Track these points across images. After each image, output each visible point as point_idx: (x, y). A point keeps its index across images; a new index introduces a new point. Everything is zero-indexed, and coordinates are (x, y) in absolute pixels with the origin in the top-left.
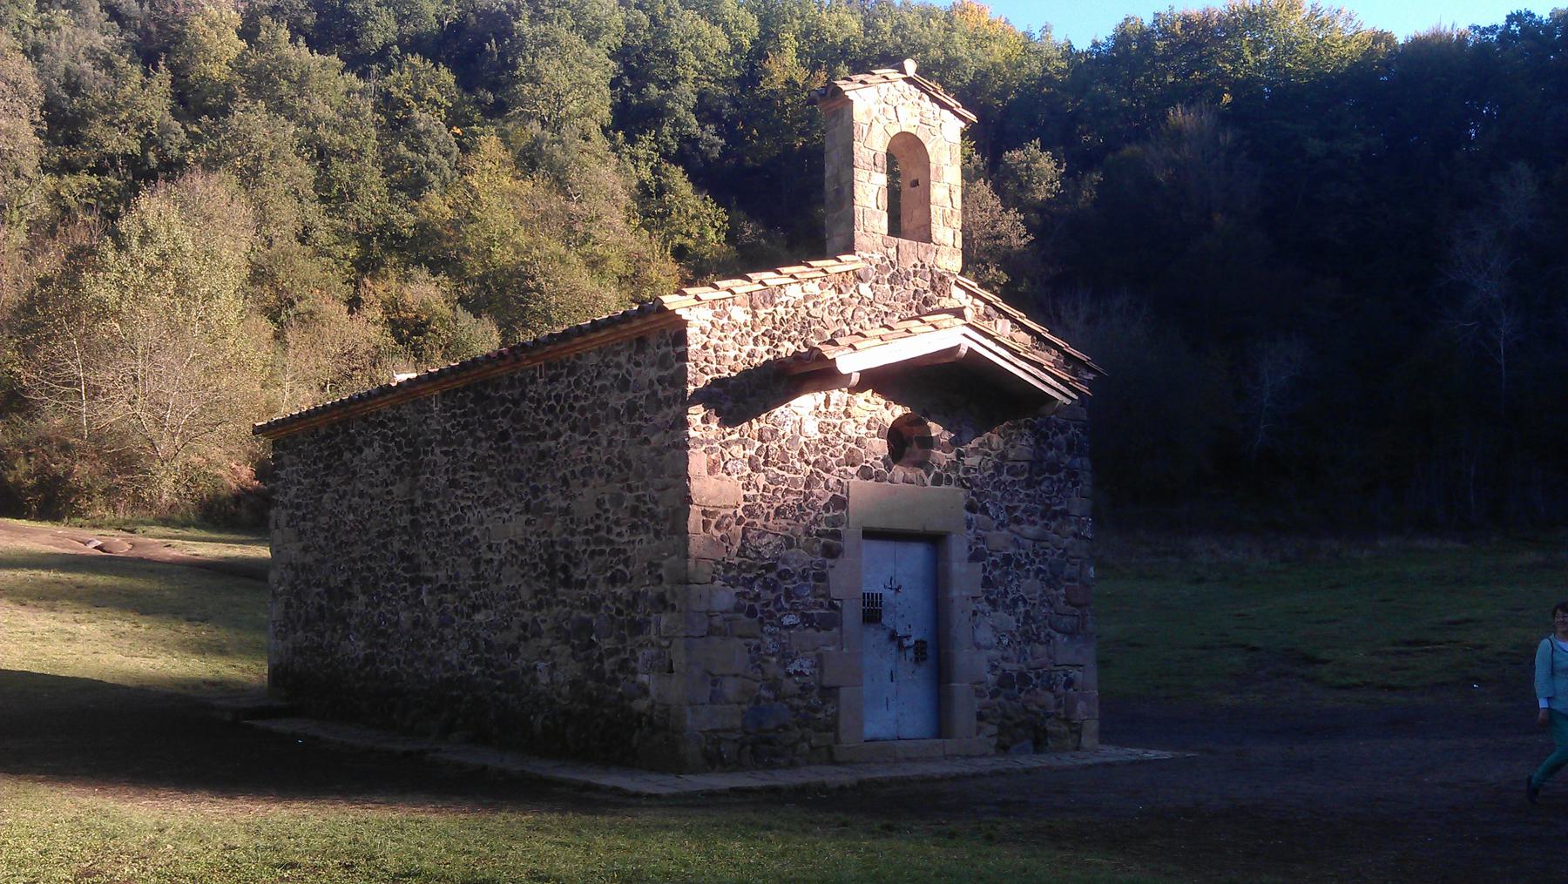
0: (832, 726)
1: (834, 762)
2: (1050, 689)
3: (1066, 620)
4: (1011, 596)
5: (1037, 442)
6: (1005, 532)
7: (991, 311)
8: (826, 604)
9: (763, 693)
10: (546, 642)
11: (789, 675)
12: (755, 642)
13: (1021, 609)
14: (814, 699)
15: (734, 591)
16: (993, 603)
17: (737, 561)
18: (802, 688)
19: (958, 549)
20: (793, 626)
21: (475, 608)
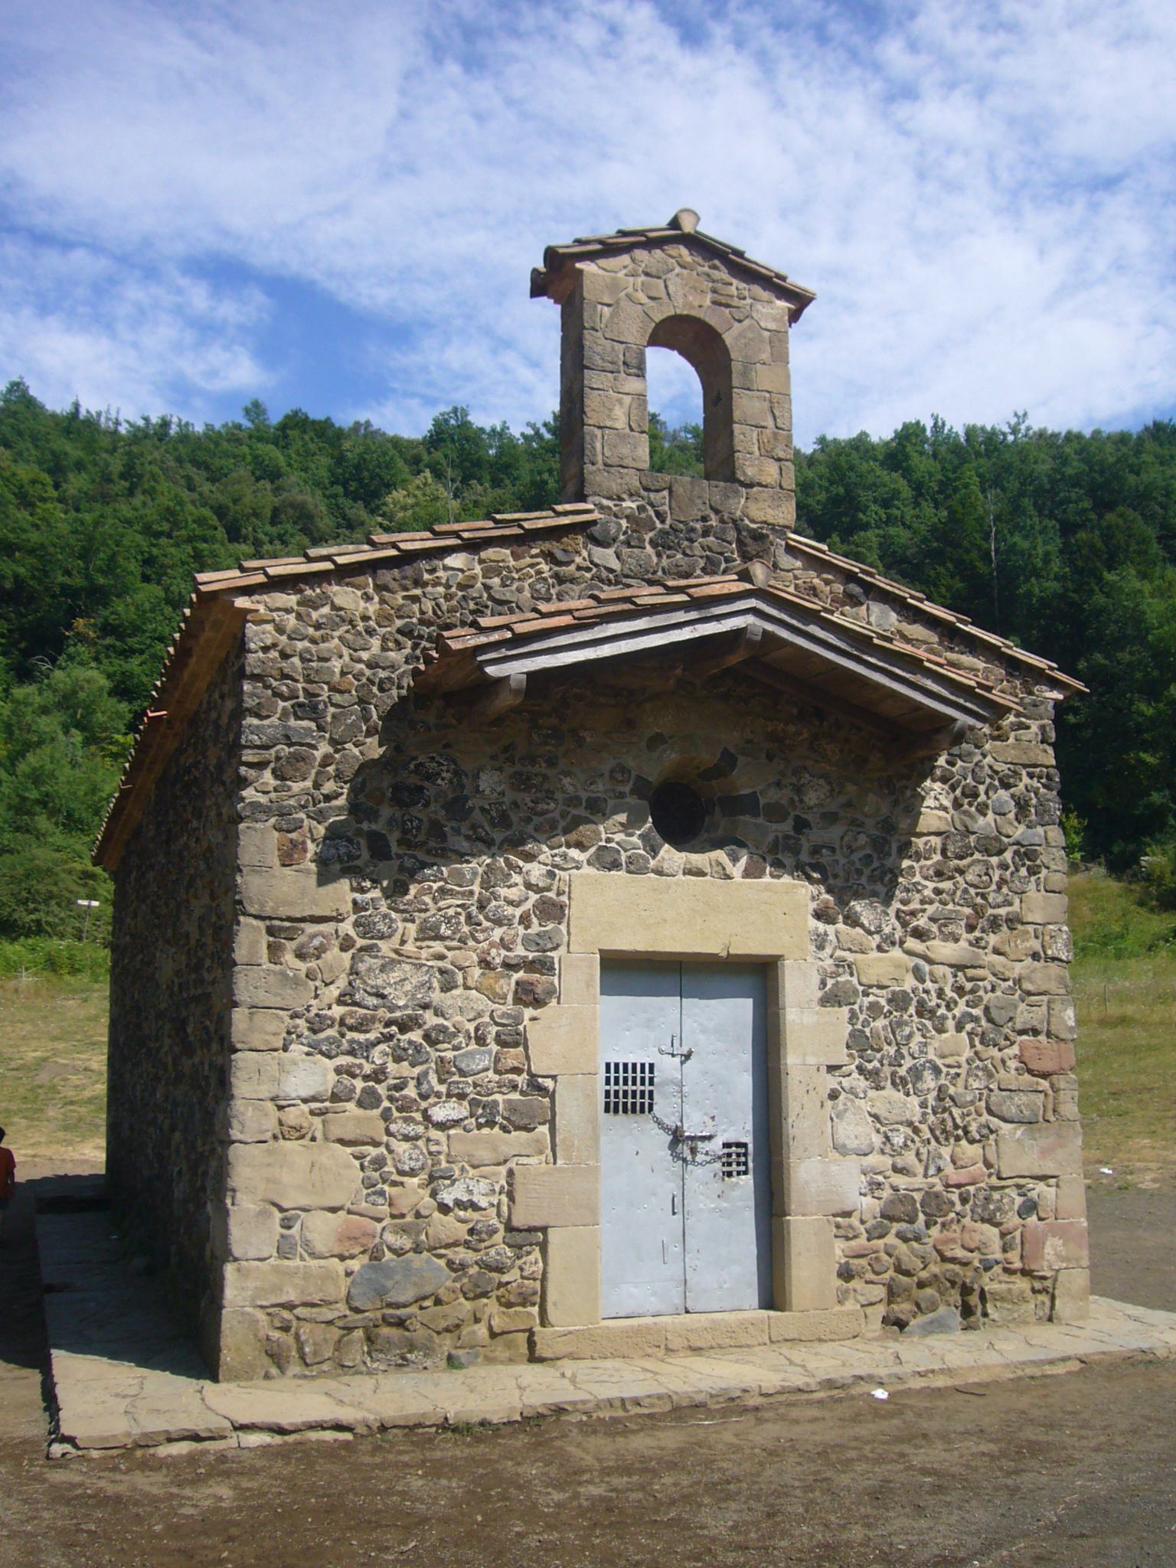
1: (534, 1358)
2: (990, 1221)
3: (1021, 1099)
4: (908, 1063)
5: (957, 805)
6: (896, 953)
7: (856, 589)
8: (521, 1080)
9: (389, 1238)
11: (444, 1209)
12: (373, 1151)
13: (929, 1081)
14: (498, 1248)
15: (330, 1064)
16: (873, 1076)
17: (338, 1011)
18: (471, 1231)
19: (799, 988)
20: (456, 1123)
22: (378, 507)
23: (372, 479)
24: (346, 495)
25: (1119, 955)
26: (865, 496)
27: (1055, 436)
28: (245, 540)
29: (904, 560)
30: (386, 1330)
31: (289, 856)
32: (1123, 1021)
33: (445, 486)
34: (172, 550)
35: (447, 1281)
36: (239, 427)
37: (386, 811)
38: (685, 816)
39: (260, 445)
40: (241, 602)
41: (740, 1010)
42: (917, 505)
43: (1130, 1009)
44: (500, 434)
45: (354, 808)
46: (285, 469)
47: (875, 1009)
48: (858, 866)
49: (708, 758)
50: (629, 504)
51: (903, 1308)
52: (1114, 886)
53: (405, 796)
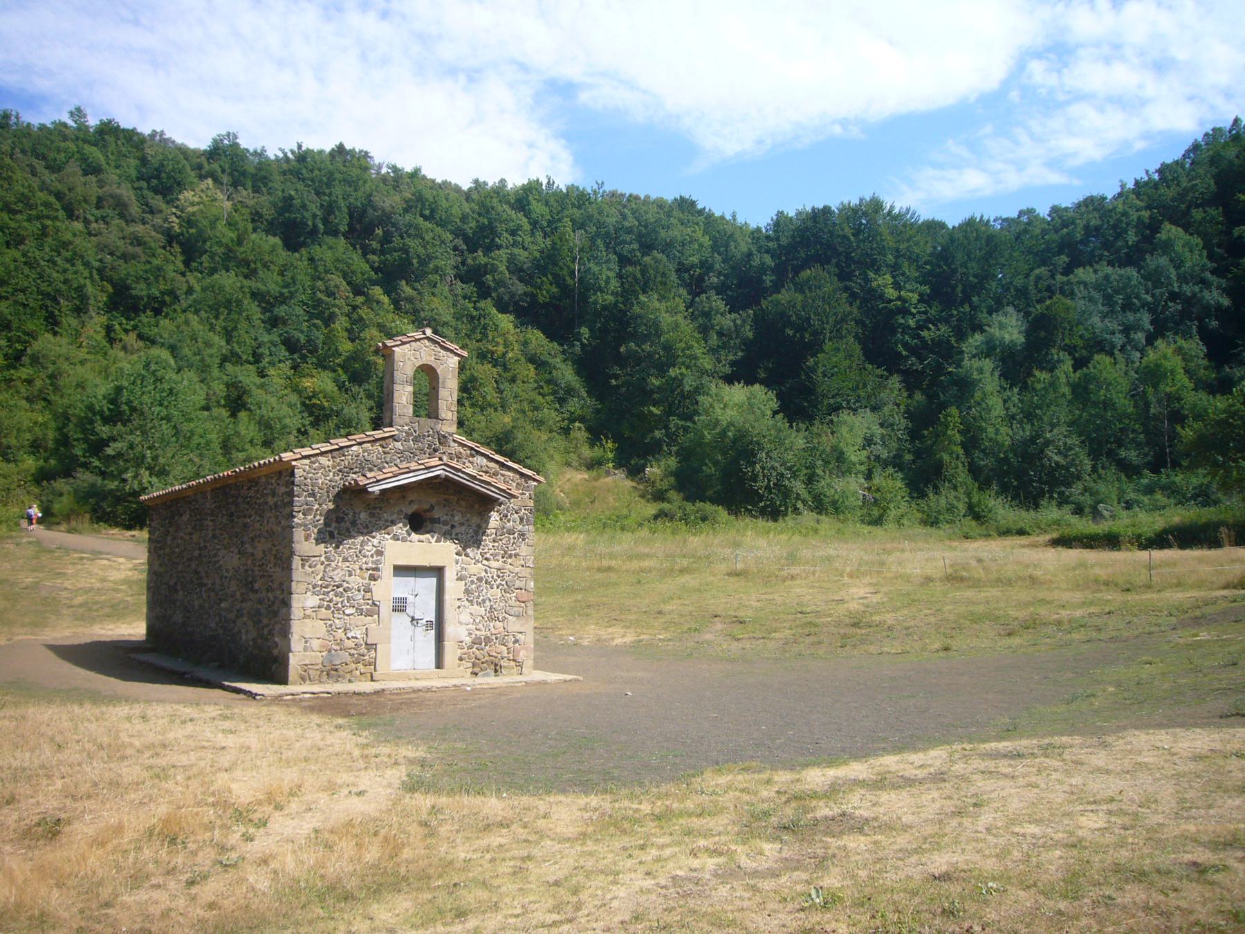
0: (374, 664)
10: (245, 619)
14: (363, 650)
21: (221, 600)
22: (172, 200)
23: (168, 178)
24: (148, 189)
25: (623, 529)
26: (500, 228)
27: (622, 195)
28: (78, 218)
29: (521, 270)
30: (332, 672)
31: (307, 538)
32: (609, 569)
33: (222, 191)
34: (25, 224)
35: (349, 659)
36: (65, 125)
37: (334, 525)
38: (418, 523)
39: (86, 146)
40: (294, 463)
41: (432, 582)
42: (533, 234)
43: (613, 563)
44: (260, 154)
45: (326, 524)
46: (105, 166)
47: (472, 582)
48: (471, 538)
49: (426, 506)
50: (406, 428)
51: (476, 670)
52: (629, 483)
53: (340, 520)
